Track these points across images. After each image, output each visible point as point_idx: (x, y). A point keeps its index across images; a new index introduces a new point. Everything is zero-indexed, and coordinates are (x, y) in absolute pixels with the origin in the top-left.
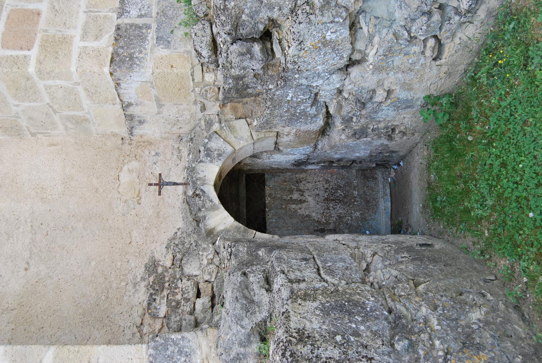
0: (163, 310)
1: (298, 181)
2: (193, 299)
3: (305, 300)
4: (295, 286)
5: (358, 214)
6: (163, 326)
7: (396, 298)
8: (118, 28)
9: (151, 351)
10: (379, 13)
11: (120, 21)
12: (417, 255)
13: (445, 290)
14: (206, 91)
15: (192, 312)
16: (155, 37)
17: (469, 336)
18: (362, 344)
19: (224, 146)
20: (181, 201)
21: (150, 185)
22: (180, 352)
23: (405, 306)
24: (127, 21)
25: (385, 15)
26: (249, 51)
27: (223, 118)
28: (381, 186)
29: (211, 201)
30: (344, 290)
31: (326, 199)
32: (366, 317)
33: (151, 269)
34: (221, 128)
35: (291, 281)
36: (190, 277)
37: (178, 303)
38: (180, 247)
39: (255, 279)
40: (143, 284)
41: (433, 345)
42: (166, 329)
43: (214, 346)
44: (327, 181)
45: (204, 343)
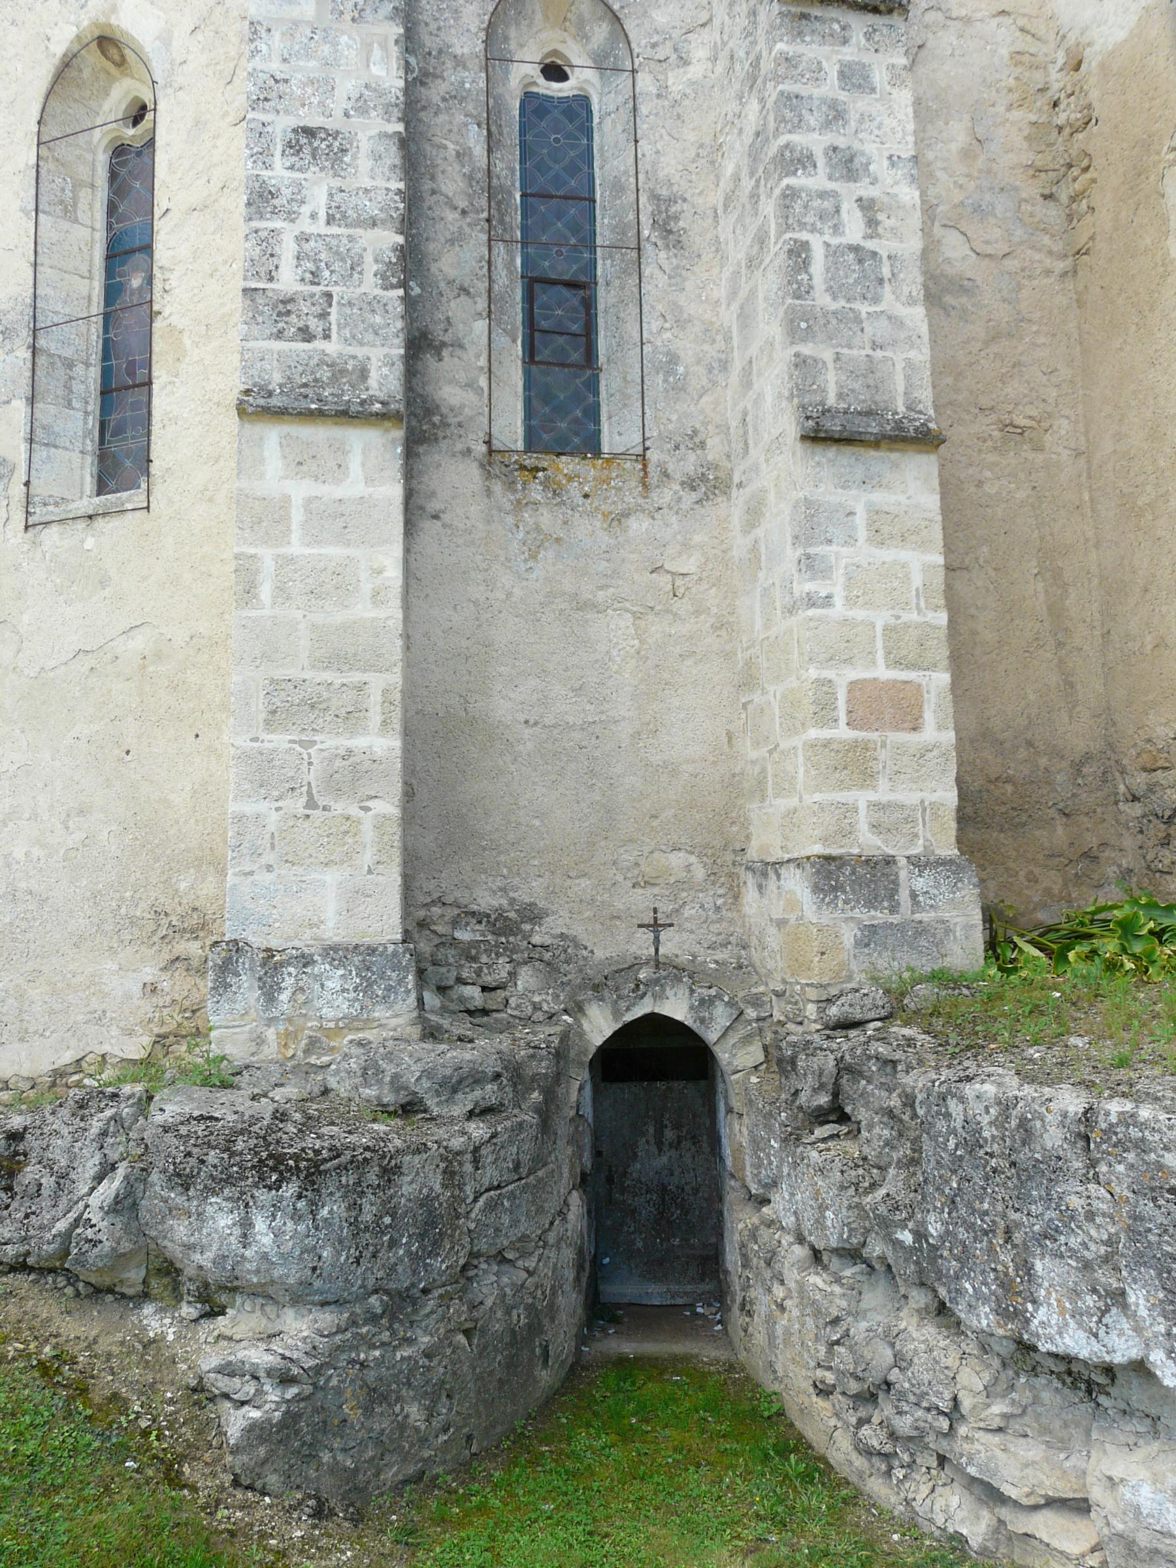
0: (463, 935)
1: (695, 1139)
2: (480, 982)
3: (444, 1172)
4: (469, 1156)
5: (640, 1244)
6: (441, 936)
7: (446, 1301)
8: (889, 861)
9: (391, 948)
10: (866, 1296)
11: (903, 862)
12: (524, 1341)
13: (454, 1373)
14: (796, 1003)
15: (460, 981)
16: (875, 922)
17: (384, 1398)
18: (378, 1251)
19: (718, 1027)
20: (639, 953)
21: (655, 911)
22: (389, 989)
23: (432, 1312)
24: (903, 875)
25: (863, 1305)
26: (822, 1086)
27: (766, 1024)
28: (689, 1288)
29: (628, 1009)
30: (458, 1227)
31: (664, 1188)
32: (415, 1258)
33: (528, 913)
34: (749, 1022)
35: (476, 1149)
36: (513, 975)
37: (474, 959)
38: (563, 956)
39: (489, 1093)
40: (504, 902)
41: (375, 1347)
42: (437, 941)
43: (396, 1035)
44: (696, 1191)
45: (400, 1021)
